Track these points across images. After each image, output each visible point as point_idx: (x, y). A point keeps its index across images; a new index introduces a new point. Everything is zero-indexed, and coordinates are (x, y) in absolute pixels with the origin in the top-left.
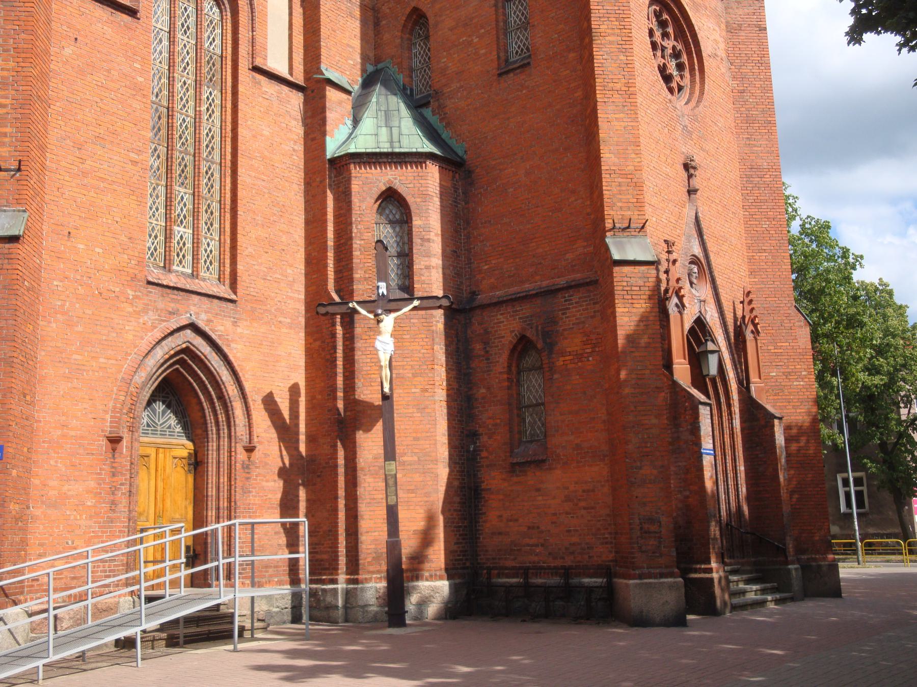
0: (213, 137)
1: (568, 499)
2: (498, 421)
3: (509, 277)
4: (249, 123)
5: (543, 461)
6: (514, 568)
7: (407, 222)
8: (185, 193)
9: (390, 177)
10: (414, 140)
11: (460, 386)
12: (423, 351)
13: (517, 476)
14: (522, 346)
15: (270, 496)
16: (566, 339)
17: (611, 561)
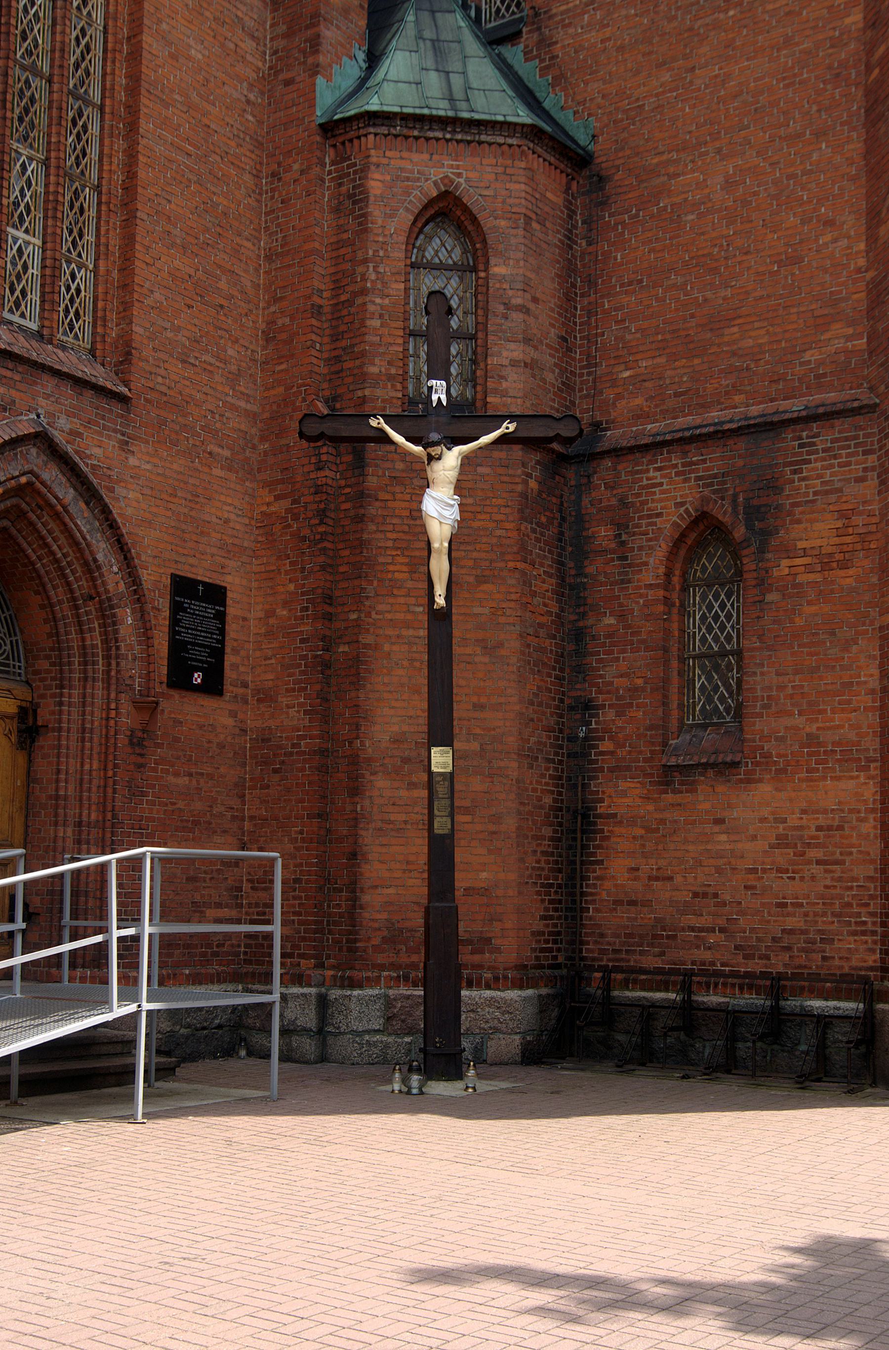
0: (88, 48)
1: (782, 842)
2: (640, 682)
3: (677, 395)
4: (164, 26)
5: (735, 765)
6: (659, 971)
7: (474, 270)
8: (31, 159)
9: (449, 172)
10: (496, 102)
11: (562, 610)
12: (499, 532)
13: (674, 792)
14: (703, 532)
15: (181, 804)
16: (799, 522)
17: (871, 969)
